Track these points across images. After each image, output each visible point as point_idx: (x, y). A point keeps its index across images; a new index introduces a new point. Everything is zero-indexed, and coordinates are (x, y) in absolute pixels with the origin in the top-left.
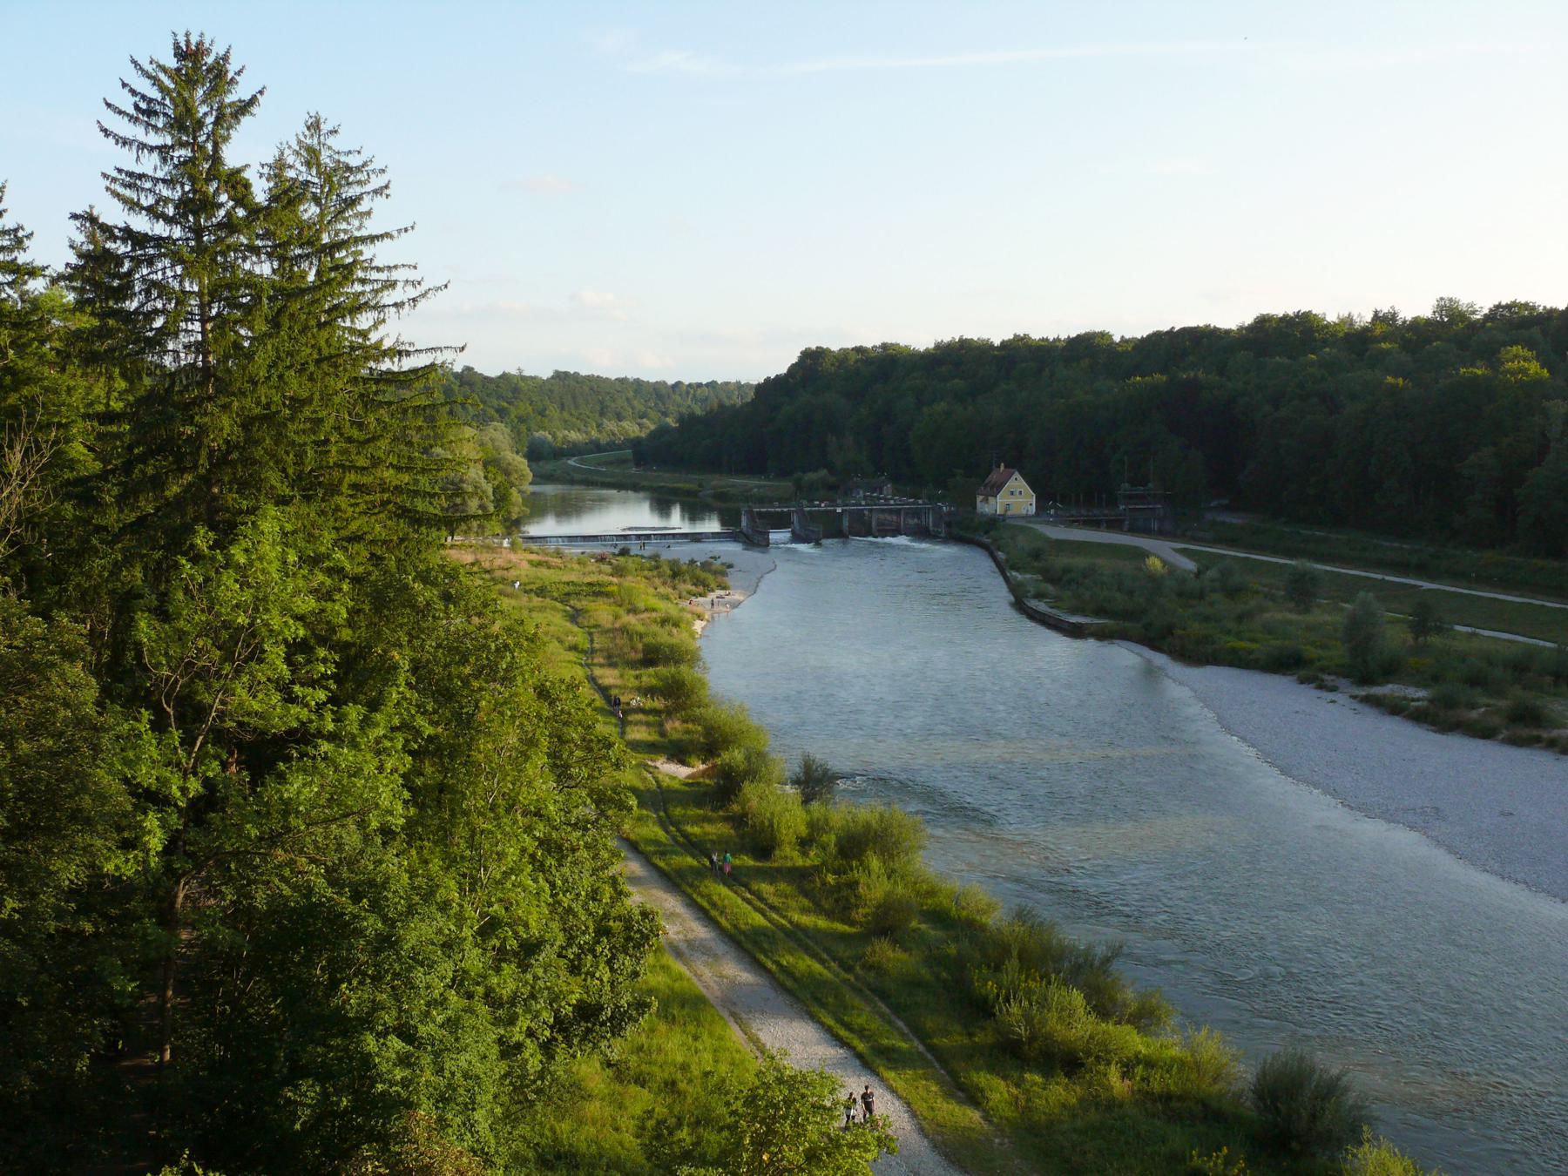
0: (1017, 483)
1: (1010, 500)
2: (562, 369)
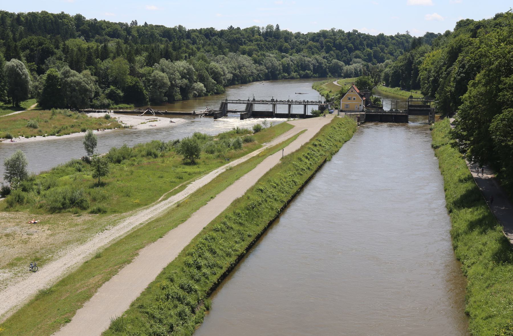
0: (352, 93)
1: (349, 102)
2: (430, 32)
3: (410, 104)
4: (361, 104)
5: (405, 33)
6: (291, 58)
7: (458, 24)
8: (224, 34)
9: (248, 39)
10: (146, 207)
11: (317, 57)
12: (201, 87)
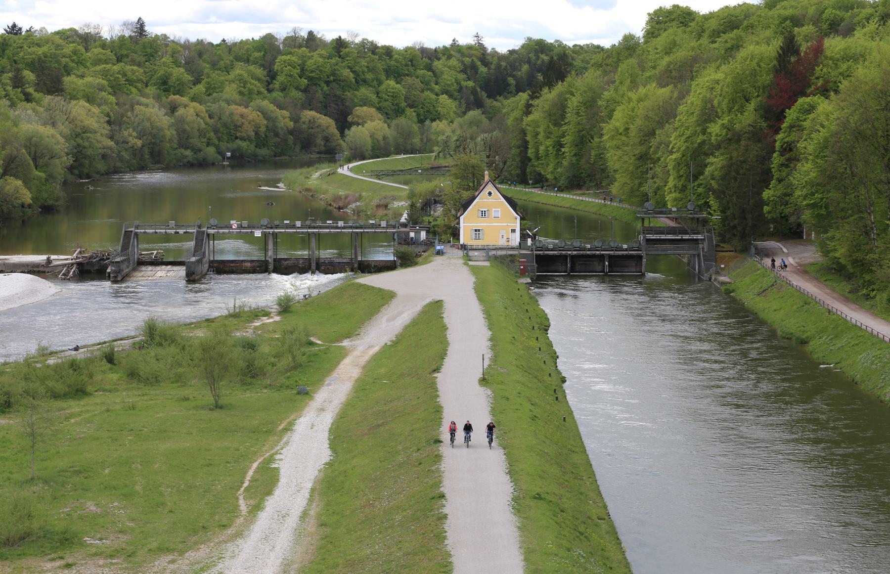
0: (490, 200)
1: (481, 224)
3: (646, 224)
4: (516, 226)
5: (471, 41)
6: (194, 108)
7: (652, 18)
8: (10, 46)
9: (75, 57)
10: (229, 531)
11: (265, 104)
12: (17, 190)
